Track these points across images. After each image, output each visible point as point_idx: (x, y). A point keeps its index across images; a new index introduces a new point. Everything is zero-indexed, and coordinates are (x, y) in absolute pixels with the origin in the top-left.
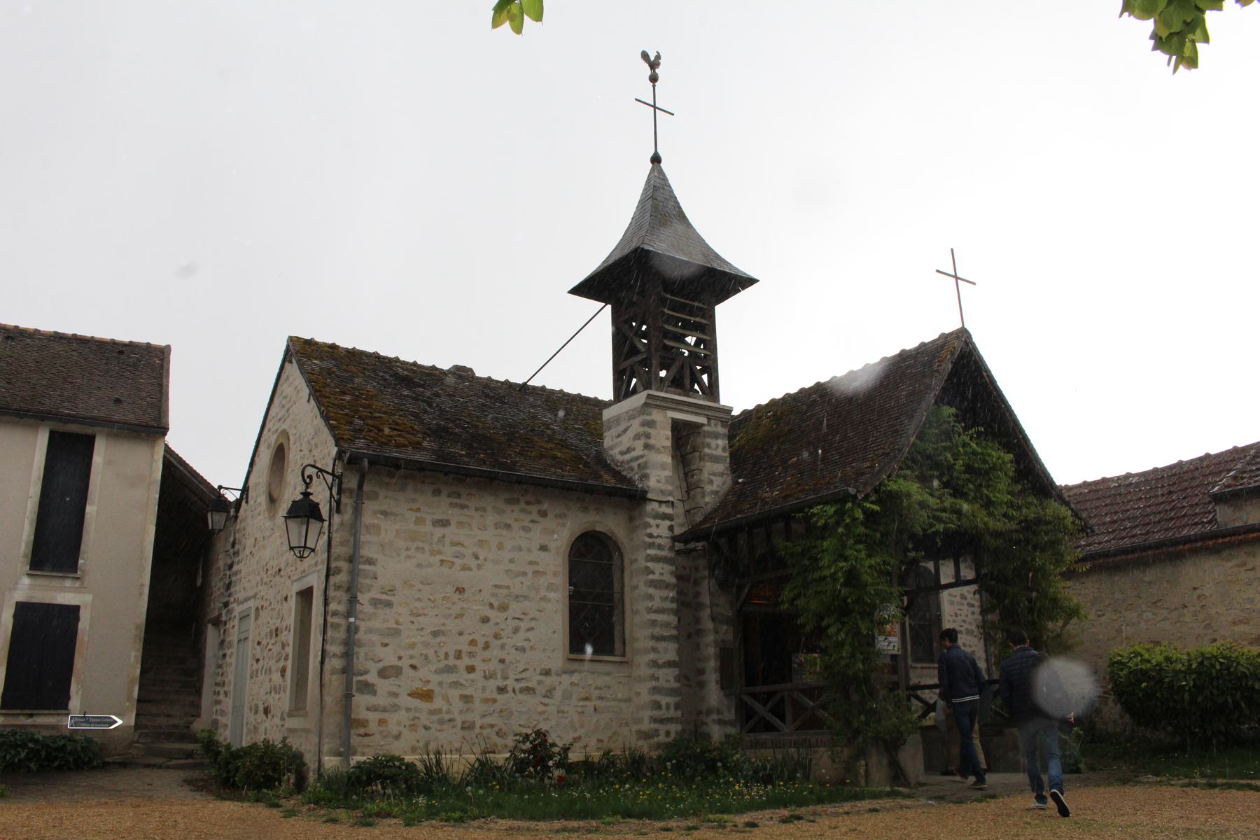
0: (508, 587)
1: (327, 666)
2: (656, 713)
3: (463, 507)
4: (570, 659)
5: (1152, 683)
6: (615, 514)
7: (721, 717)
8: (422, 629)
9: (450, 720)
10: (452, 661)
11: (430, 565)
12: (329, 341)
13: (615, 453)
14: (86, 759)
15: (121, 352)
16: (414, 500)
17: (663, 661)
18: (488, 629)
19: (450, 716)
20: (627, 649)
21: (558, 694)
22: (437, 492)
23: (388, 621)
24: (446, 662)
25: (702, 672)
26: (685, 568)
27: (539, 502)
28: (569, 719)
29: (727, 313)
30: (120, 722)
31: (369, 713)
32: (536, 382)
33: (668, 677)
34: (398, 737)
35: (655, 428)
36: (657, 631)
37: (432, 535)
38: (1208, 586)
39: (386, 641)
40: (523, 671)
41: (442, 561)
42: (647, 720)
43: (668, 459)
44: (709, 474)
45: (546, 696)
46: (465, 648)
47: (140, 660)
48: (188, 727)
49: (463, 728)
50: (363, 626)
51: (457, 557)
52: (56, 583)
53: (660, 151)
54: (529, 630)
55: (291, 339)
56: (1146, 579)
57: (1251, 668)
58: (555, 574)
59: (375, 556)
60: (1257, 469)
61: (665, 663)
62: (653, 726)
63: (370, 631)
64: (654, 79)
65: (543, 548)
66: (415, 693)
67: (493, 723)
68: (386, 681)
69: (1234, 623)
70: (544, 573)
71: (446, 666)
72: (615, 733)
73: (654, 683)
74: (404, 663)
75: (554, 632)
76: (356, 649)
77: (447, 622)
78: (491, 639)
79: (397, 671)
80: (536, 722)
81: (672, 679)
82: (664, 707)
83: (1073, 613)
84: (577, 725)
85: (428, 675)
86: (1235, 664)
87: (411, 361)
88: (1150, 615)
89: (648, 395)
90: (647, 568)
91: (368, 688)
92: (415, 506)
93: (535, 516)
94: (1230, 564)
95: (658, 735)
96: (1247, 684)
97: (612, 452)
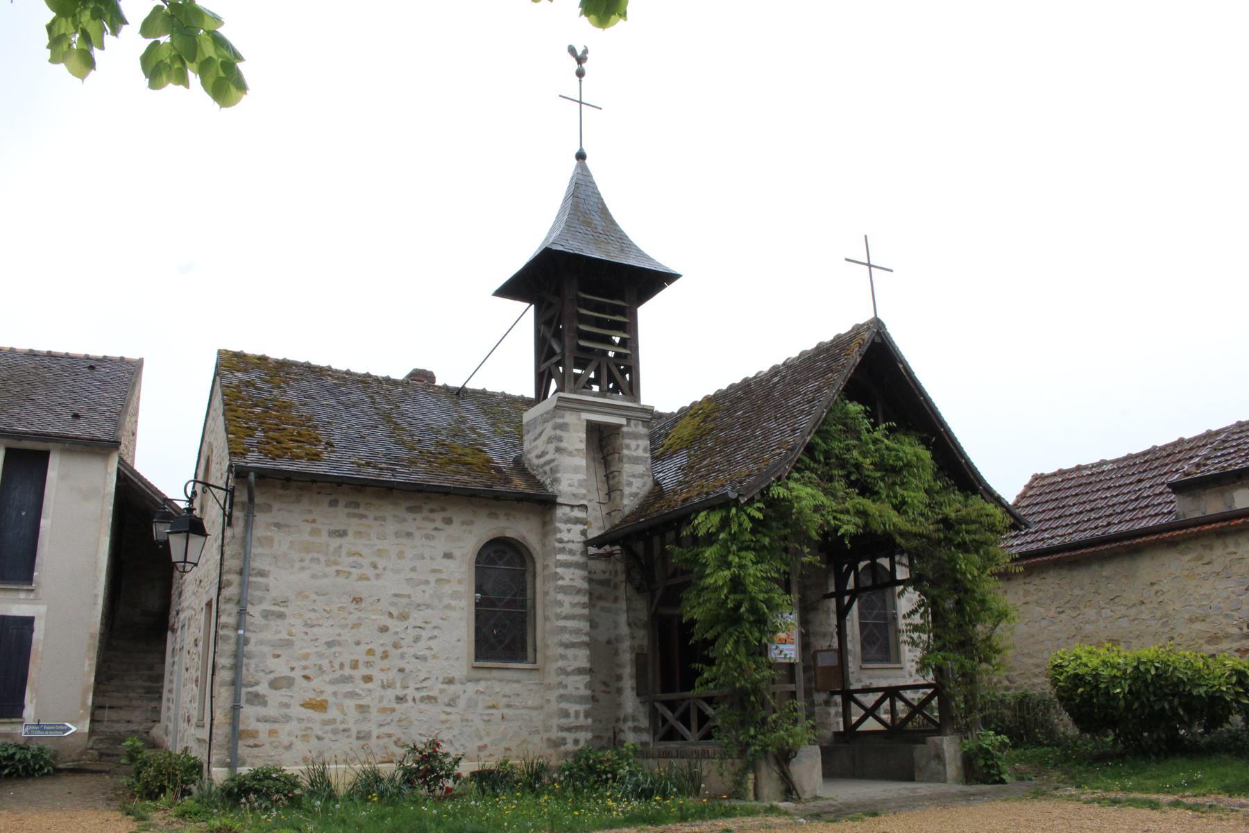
0: (409, 596)
1: (217, 679)
2: (564, 721)
3: (362, 516)
4: (475, 668)
5: (1088, 689)
6: (527, 519)
7: (636, 724)
8: (317, 639)
9: (344, 730)
10: (347, 671)
11: (326, 576)
12: (259, 353)
13: (532, 456)
14: (37, 767)
15: (92, 368)
16: (310, 512)
17: (572, 668)
18: (387, 639)
19: (345, 726)
20: (539, 656)
21: (462, 703)
22: (334, 503)
23: (280, 632)
24: (341, 672)
25: (619, 678)
26: (604, 572)
27: (443, 509)
28: (474, 728)
29: (651, 315)
30: (74, 729)
31: (259, 723)
32: (472, 385)
33: (578, 685)
34: (289, 747)
35: (568, 431)
36: (566, 638)
37: (328, 545)
38: (1165, 581)
39: (278, 652)
40: (424, 680)
41: (338, 572)
42: (555, 729)
43: (581, 462)
44: (628, 476)
45: (449, 705)
46: (362, 658)
47: (94, 668)
48: (148, 733)
49: (358, 738)
50: (253, 638)
51: (354, 567)
52: (11, 596)
54: (431, 638)
55: (220, 352)
56: (1104, 574)
57: (1189, 673)
58: (460, 582)
59: (267, 568)
60: (1247, 454)
62: (561, 734)
63: (261, 642)
64: (580, 74)
65: (448, 556)
66: (307, 704)
67: (391, 732)
69: (1191, 620)
70: (448, 581)
71: (342, 675)
72: (524, 741)
73: (562, 691)
74: (297, 675)
75: (459, 640)
76: (245, 661)
77: (342, 632)
78: (389, 648)
79: (290, 682)
80: (437, 731)
81: (582, 686)
83: (1002, 616)
84: (483, 733)
85: (322, 686)
86: (1171, 669)
87: (344, 369)
88: (1109, 613)
90: (556, 573)
91: (257, 699)
92: (310, 517)
93: (439, 524)
94: (1187, 558)
95: (565, 744)
96: (1184, 690)
97: (529, 456)
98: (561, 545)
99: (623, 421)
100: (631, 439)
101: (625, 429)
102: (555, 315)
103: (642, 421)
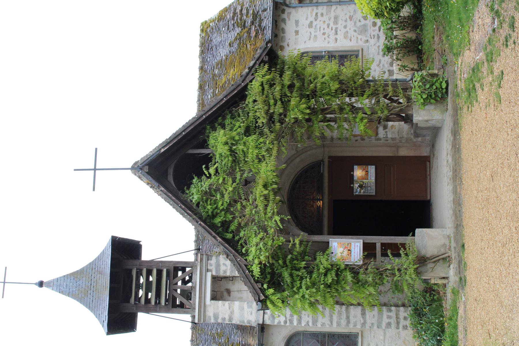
2: (393, 325)
6: (272, 334)
17: (361, 319)
33: (372, 315)
35: (218, 314)
61: (363, 318)
82: (389, 320)
98: (288, 322)
99: (209, 275)
100: (220, 269)
101: (214, 274)
103: (208, 260)
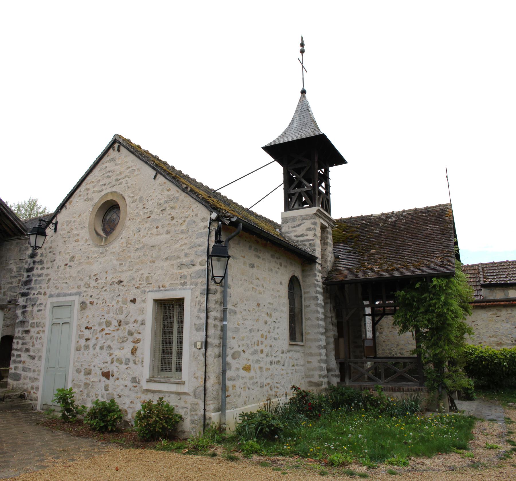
5: (487, 362)
32: (223, 192)
53: (305, 88)
68: (235, 360)
69: (490, 337)
89: (318, 209)
94: (490, 313)
102: (305, 167)
